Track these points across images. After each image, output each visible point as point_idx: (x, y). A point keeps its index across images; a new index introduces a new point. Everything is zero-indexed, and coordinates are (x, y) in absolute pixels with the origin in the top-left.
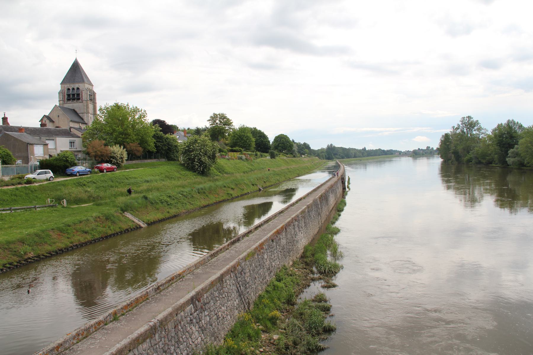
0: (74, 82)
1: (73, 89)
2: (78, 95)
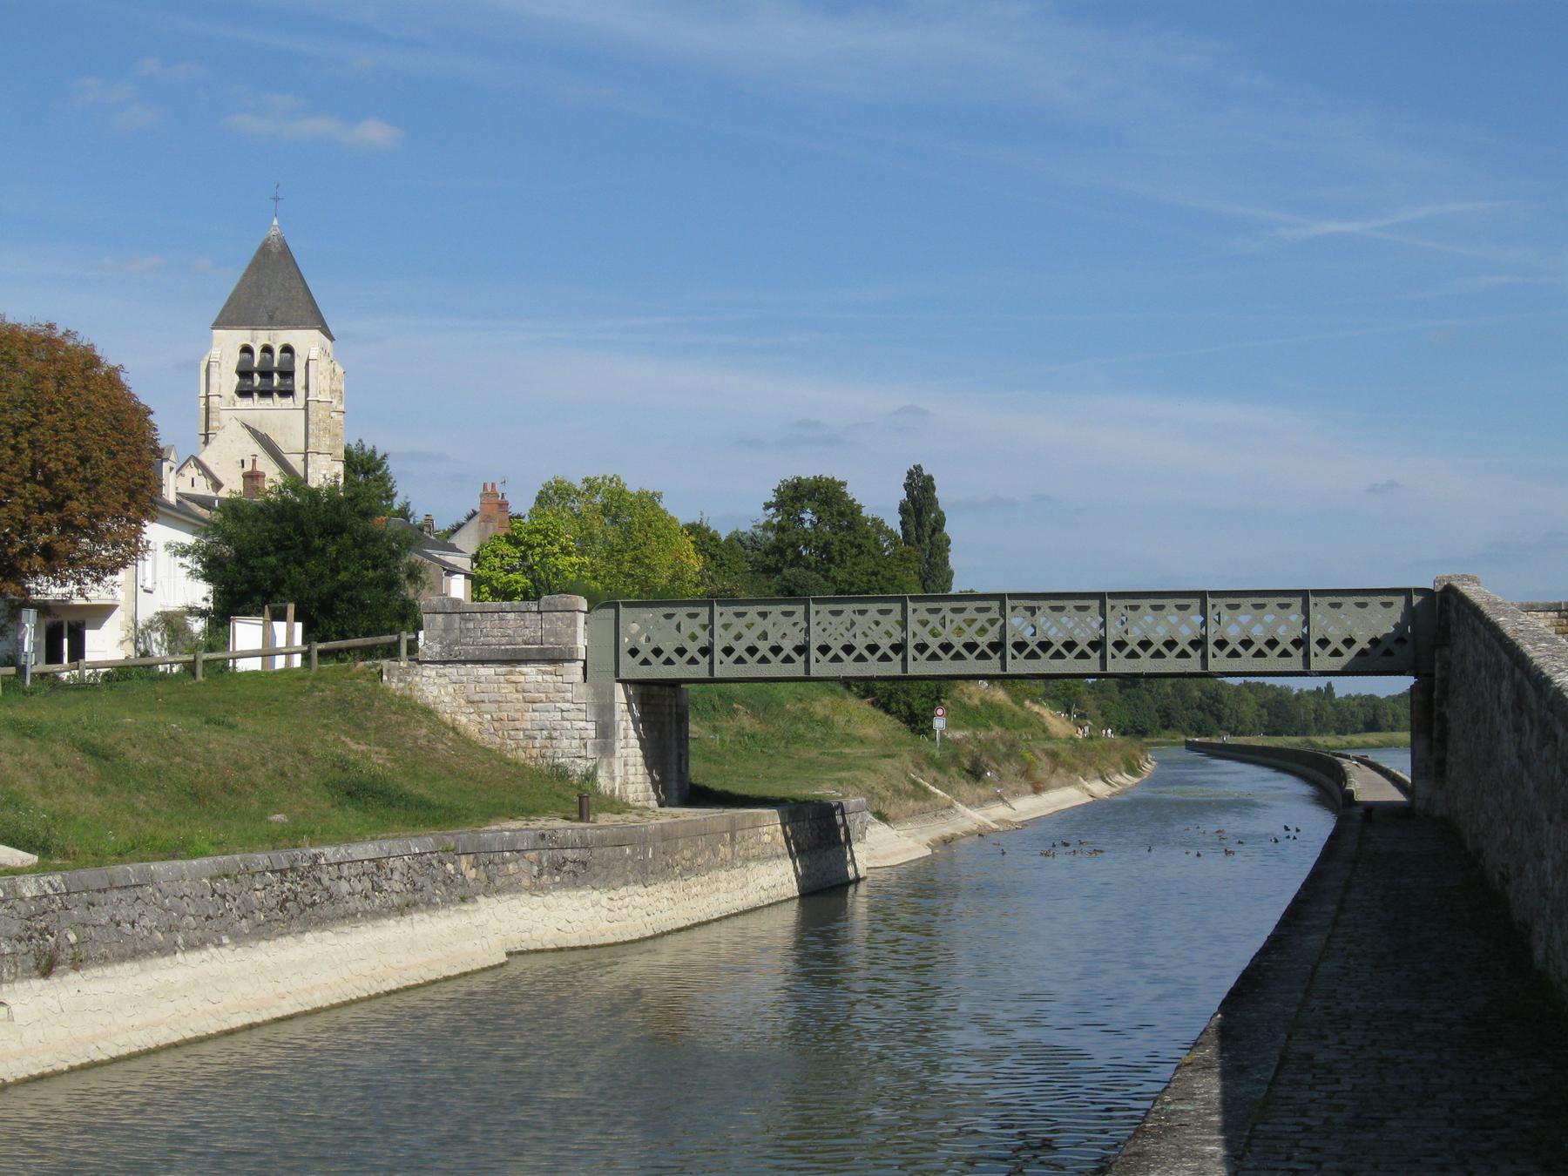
0: (274, 321)
1: (267, 349)
2: (287, 374)
